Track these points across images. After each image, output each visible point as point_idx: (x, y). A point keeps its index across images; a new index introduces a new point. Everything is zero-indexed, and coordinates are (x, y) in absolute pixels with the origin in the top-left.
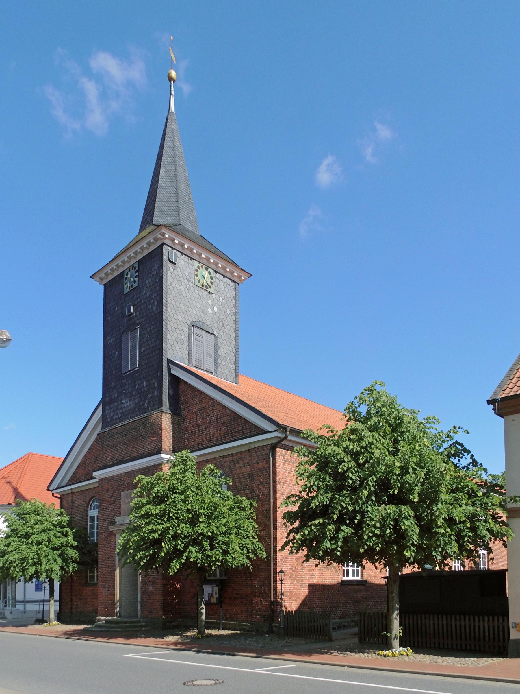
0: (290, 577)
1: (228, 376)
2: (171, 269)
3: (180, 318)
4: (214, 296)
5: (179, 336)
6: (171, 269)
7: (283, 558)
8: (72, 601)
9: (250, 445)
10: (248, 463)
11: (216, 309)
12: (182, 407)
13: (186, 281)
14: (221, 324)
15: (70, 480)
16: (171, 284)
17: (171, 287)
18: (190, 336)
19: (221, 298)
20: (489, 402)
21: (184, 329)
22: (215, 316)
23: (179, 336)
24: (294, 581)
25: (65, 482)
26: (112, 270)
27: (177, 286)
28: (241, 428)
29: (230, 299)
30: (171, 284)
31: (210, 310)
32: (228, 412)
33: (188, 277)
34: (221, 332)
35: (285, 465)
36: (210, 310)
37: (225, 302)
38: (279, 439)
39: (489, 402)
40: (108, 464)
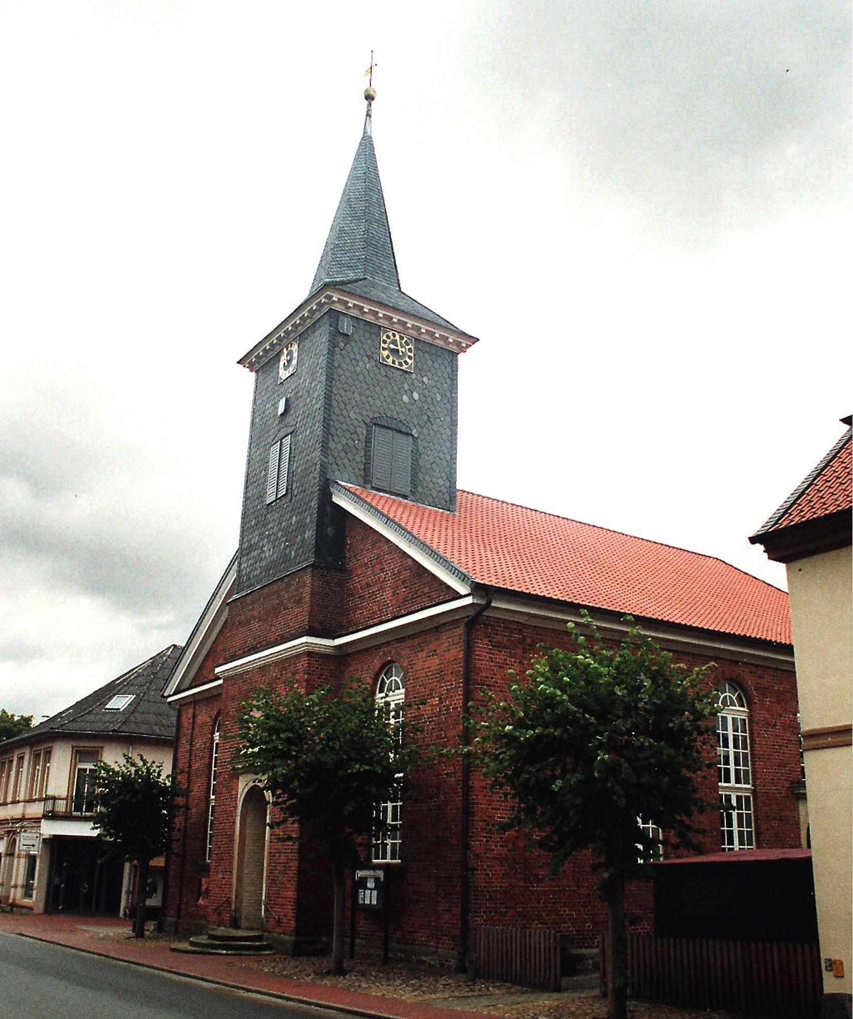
0: (501, 862)
1: (437, 500)
2: (342, 345)
3: (352, 415)
4: (414, 376)
5: (350, 442)
6: (342, 345)
7: (488, 825)
8: (181, 894)
9: (437, 619)
10: (435, 651)
11: (416, 396)
12: (348, 554)
13: (365, 358)
14: (425, 417)
15: (194, 679)
16: (339, 366)
17: (340, 371)
18: (368, 441)
19: (425, 379)
20: (753, 540)
21: (359, 430)
22: (414, 407)
23: (350, 442)
24: (511, 869)
25: (186, 684)
26: (265, 350)
27: (350, 367)
28: (426, 590)
29: (442, 380)
30: (339, 366)
31: (405, 398)
32: (410, 562)
33: (369, 353)
34: (425, 431)
35: (493, 654)
36: (405, 398)
37: (433, 383)
38: (478, 609)
39: (753, 540)
40: (238, 653)
